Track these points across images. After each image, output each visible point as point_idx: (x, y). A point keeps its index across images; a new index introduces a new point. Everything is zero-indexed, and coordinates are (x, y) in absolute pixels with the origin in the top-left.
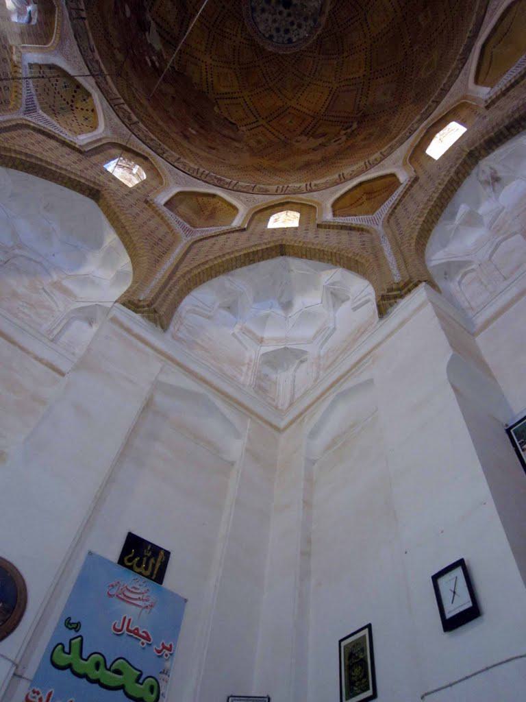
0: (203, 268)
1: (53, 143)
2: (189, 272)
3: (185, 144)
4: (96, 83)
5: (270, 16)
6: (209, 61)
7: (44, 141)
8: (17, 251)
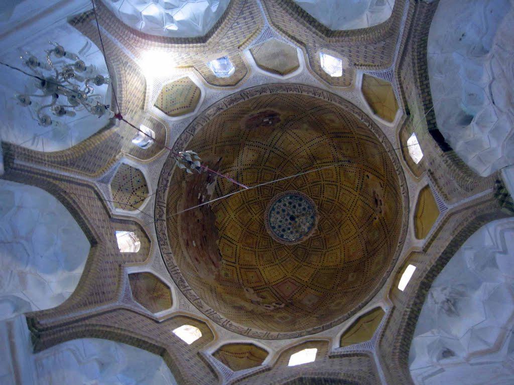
0: (105, 329)
1: (99, 203)
2: (93, 325)
3: (183, 248)
4: (157, 190)
5: (280, 218)
6: (232, 216)
7: (94, 198)
8: (23, 241)
